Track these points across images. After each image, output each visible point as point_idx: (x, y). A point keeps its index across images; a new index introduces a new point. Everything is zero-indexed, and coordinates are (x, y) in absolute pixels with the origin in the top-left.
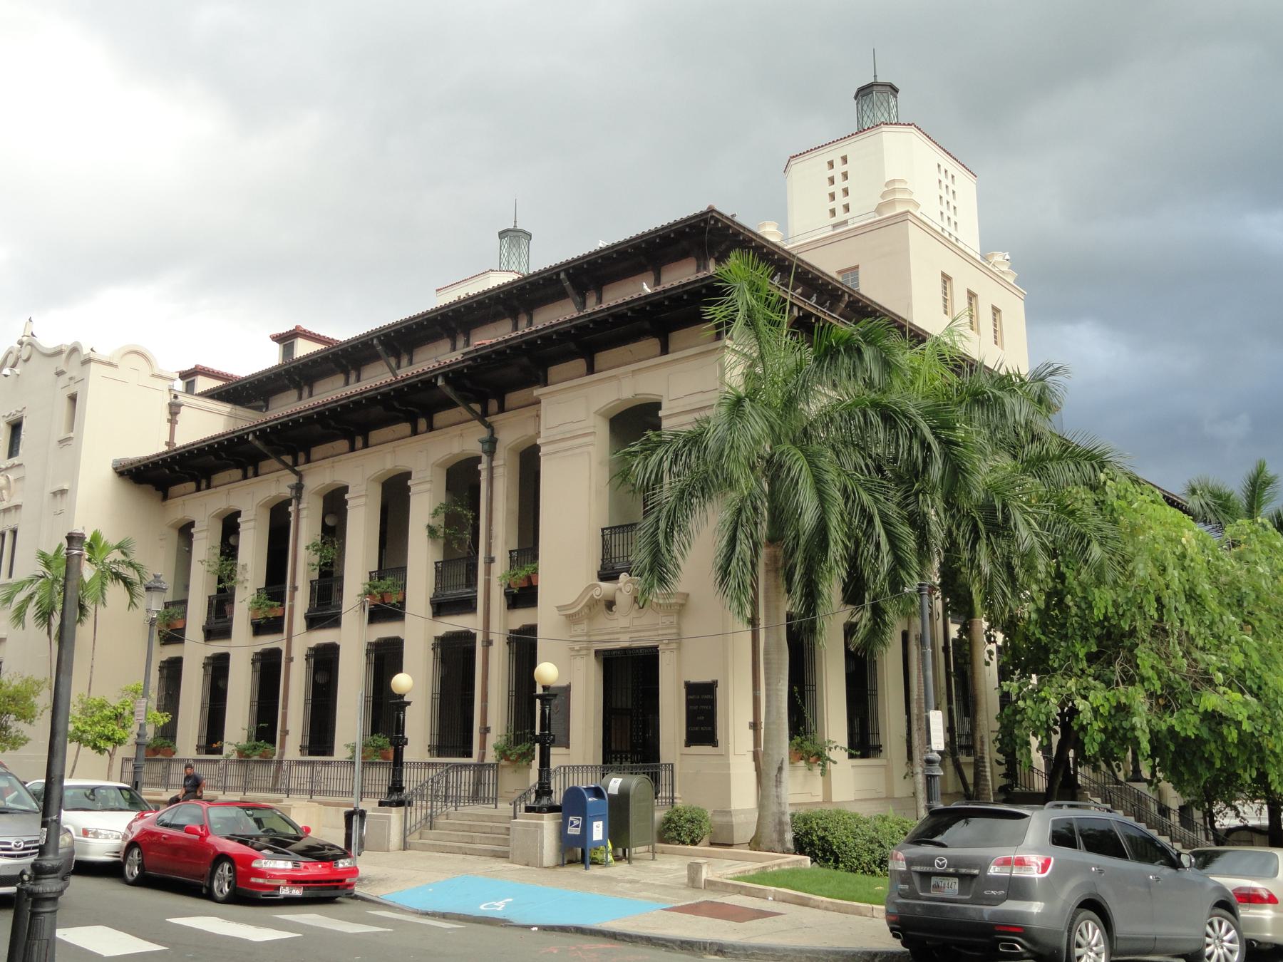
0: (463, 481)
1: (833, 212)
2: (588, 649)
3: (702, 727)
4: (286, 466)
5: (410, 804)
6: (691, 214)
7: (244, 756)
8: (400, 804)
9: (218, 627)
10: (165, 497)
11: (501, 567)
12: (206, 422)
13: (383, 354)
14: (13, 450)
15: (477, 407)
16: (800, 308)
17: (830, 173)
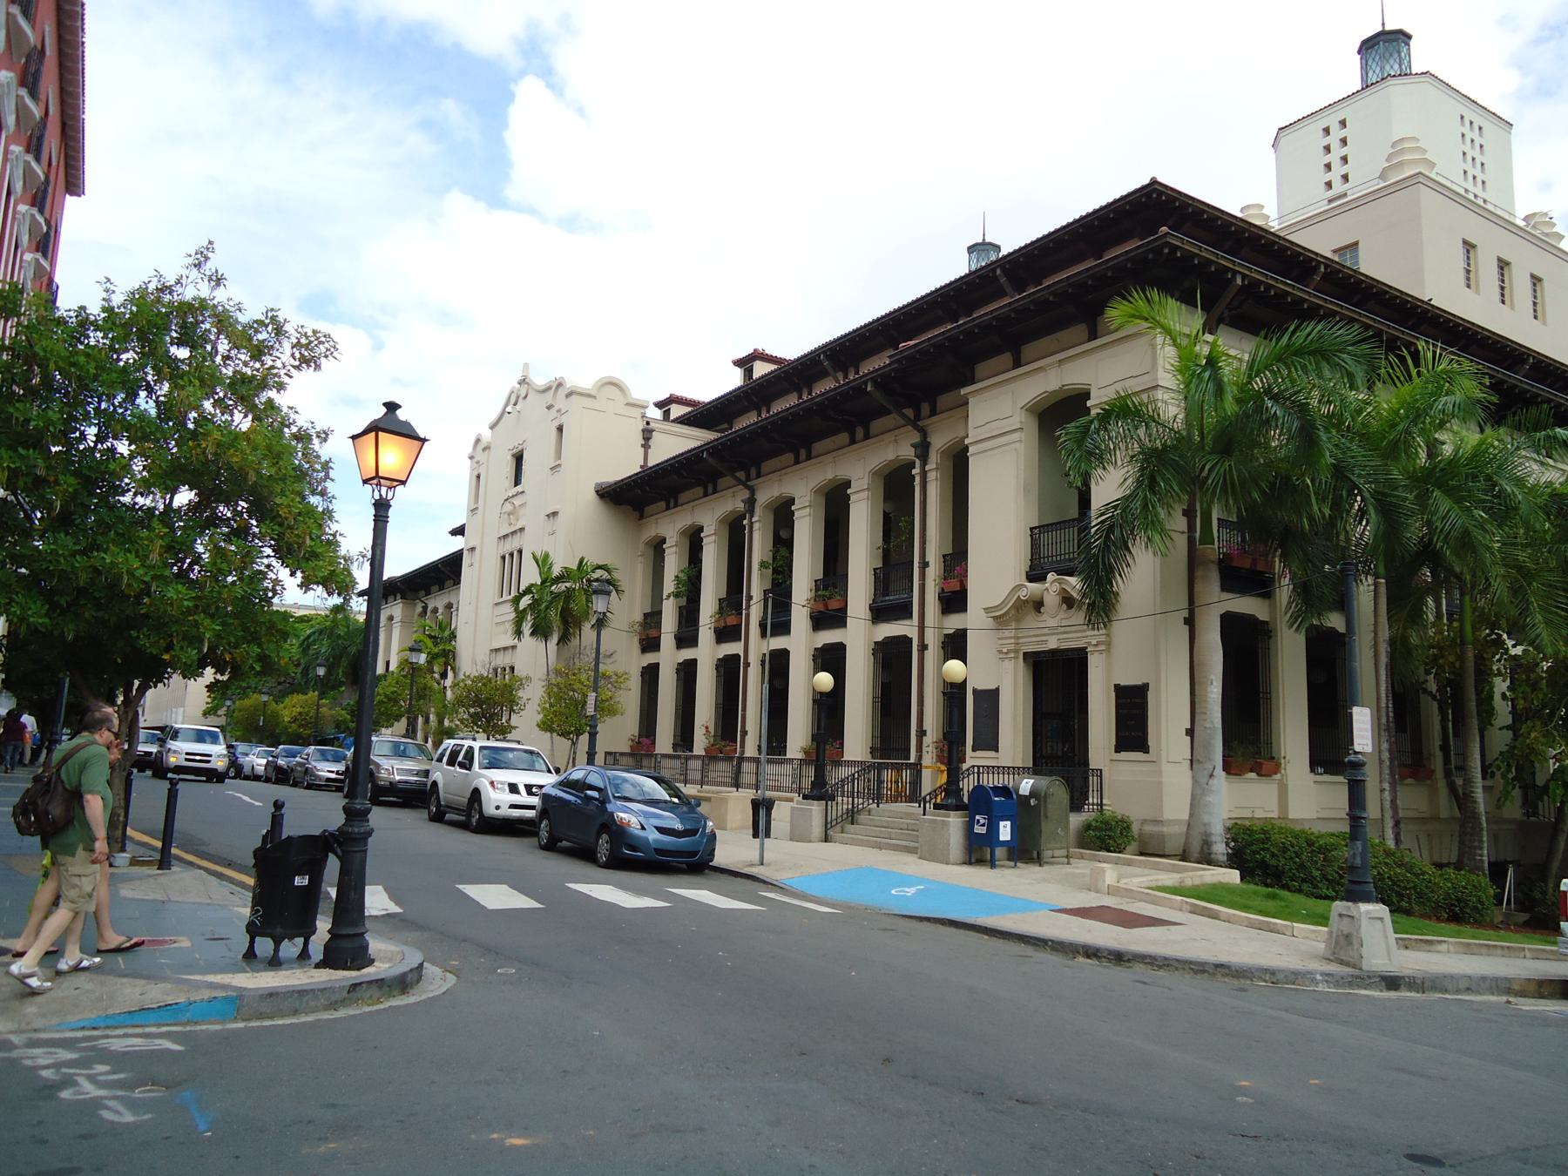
0: (897, 489)
1: (1329, 185)
2: (1016, 651)
3: (1133, 730)
4: (740, 482)
5: (833, 798)
6: (1131, 189)
7: (711, 756)
8: (819, 798)
9: (687, 637)
10: (642, 517)
11: (934, 572)
12: (674, 443)
13: (830, 370)
14: (517, 482)
15: (909, 412)
16: (1244, 276)
17: (1326, 141)
